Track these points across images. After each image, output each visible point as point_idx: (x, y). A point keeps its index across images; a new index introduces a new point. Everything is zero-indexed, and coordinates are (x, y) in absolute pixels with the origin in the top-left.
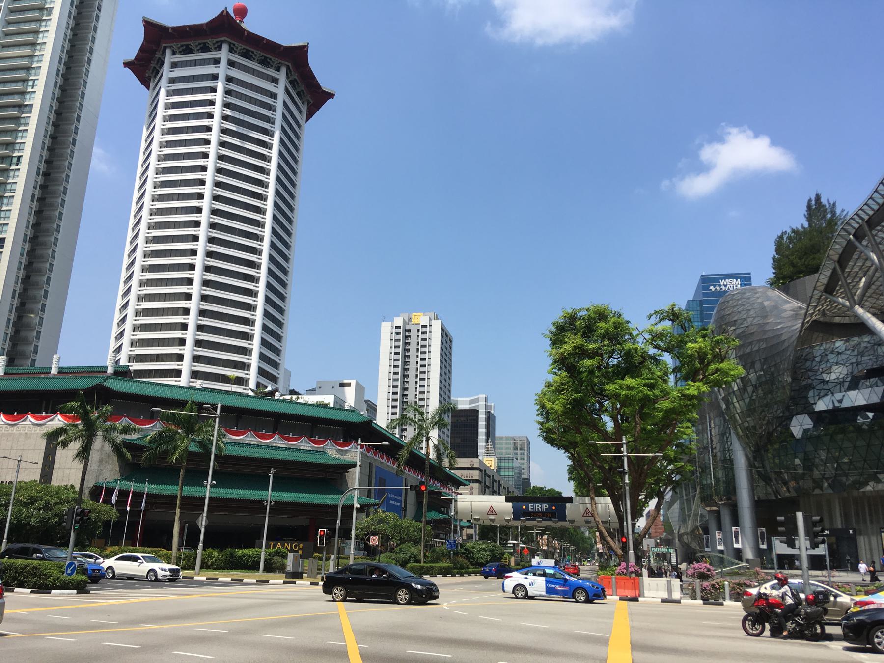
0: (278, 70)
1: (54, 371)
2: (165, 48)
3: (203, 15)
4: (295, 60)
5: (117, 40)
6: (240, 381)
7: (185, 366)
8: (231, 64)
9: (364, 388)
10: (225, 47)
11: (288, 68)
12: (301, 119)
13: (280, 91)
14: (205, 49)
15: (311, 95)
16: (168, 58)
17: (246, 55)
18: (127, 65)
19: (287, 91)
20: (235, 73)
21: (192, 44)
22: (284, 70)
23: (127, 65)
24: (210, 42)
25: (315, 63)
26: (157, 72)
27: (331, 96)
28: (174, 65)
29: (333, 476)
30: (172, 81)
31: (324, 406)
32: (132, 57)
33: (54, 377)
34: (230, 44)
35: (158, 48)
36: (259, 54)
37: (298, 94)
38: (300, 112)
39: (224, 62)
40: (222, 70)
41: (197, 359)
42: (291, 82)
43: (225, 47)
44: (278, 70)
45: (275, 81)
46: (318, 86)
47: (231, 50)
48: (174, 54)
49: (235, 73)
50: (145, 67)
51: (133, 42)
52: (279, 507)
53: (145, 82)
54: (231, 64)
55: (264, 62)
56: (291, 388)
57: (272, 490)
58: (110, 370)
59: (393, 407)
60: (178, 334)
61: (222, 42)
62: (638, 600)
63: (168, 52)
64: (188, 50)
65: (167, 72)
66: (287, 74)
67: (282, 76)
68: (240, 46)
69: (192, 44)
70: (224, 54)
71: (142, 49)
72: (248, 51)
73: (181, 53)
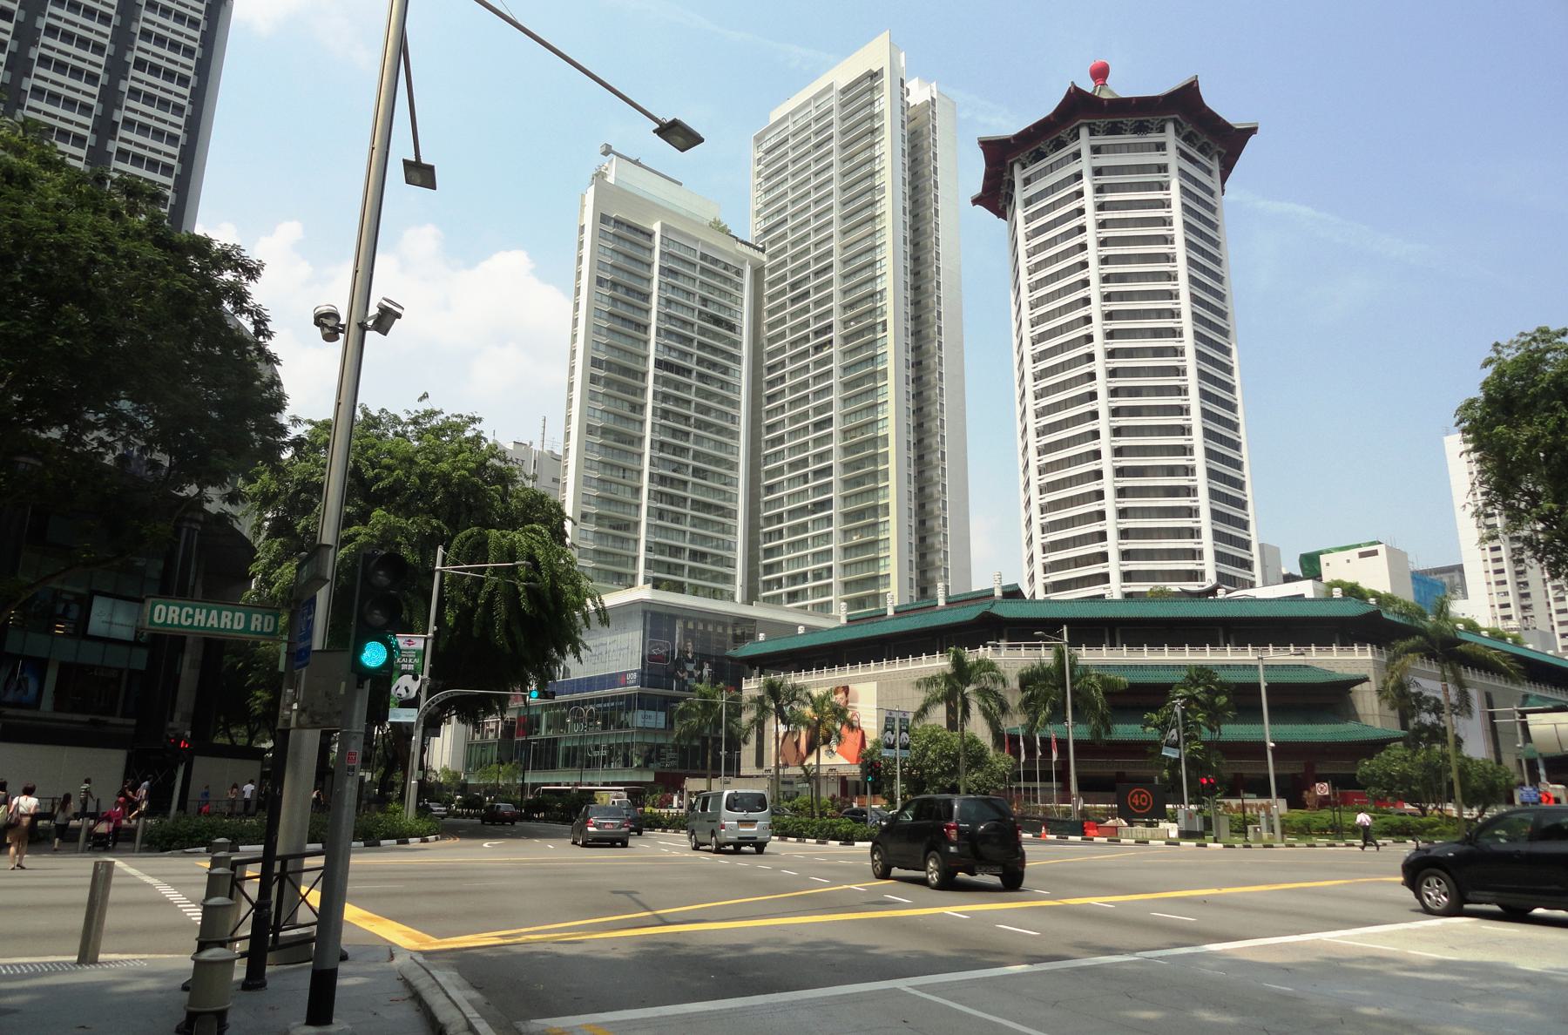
0: (1162, 130)
1: (890, 612)
2: (1012, 165)
3: (1045, 105)
4: (1184, 108)
5: (960, 173)
6: (1194, 576)
7: (1114, 567)
8: (1096, 150)
9: (1405, 554)
10: (1084, 132)
11: (1176, 122)
12: (1213, 183)
13: (1171, 158)
14: (1060, 145)
15: (1218, 141)
16: (1019, 175)
17: (1114, 130)
18: (976, 201)
19: (1183, 154)
20: (1104, 160)
21: (1042, 145)
22: (1170, 128)
23: (976, 201)
24: (1063, 134)
25: (1213, 100)
26: (1010, 198)
27: (1252, 131)
28: (1027, 181)
29: (1332, 697)
30: (1028, 202)
31: (1299, 598)
32: (977, 189)
33: (891, 619)
34: (1088, 125)
35: (1005, 162)
36: (1130, 121)
37: (1201, 150)
38: (1209, 172)
39: (1086, 153)
40: (1086, 164)
41: (1126, 555)
42: (1185, 139)
43: (1084, 132)
44: (1162, 130)
45: (1161, 147)
46: (1229, 127)
47: (1092, 133)
48: (1024, 167)
49: (1104, 160)
50: (995, 196)
51: (972, 172)
52: (1282, 750)
53: (1001, 214)
54: (1096, 150)
55: (1141, 129)
56: (1285, 571)
57: (1271, 722)
58: (998, 593)
59: (1497, 572)
60: (1094, 527)
61: (1078, 128)
62: (625, 845)
63: (1017, 167)
64: (1040, 156)
65: (1020, 194)
66: (1176, 131)
67: (1170, 137)
68: (1101, 122)
69: (1042, 145)
70: (1085, 142)
71: (987, 177)
72: (1114, 124)
73: (1031, 163)
